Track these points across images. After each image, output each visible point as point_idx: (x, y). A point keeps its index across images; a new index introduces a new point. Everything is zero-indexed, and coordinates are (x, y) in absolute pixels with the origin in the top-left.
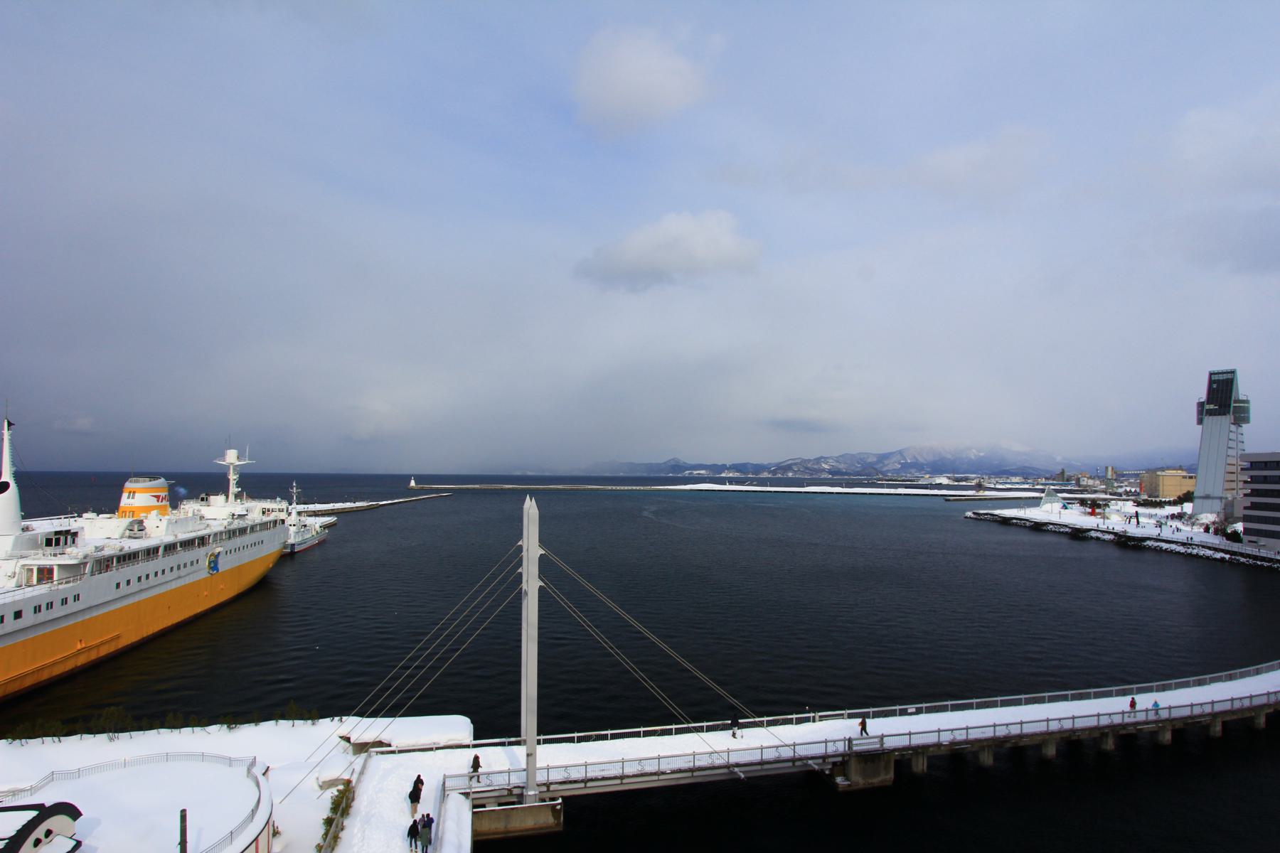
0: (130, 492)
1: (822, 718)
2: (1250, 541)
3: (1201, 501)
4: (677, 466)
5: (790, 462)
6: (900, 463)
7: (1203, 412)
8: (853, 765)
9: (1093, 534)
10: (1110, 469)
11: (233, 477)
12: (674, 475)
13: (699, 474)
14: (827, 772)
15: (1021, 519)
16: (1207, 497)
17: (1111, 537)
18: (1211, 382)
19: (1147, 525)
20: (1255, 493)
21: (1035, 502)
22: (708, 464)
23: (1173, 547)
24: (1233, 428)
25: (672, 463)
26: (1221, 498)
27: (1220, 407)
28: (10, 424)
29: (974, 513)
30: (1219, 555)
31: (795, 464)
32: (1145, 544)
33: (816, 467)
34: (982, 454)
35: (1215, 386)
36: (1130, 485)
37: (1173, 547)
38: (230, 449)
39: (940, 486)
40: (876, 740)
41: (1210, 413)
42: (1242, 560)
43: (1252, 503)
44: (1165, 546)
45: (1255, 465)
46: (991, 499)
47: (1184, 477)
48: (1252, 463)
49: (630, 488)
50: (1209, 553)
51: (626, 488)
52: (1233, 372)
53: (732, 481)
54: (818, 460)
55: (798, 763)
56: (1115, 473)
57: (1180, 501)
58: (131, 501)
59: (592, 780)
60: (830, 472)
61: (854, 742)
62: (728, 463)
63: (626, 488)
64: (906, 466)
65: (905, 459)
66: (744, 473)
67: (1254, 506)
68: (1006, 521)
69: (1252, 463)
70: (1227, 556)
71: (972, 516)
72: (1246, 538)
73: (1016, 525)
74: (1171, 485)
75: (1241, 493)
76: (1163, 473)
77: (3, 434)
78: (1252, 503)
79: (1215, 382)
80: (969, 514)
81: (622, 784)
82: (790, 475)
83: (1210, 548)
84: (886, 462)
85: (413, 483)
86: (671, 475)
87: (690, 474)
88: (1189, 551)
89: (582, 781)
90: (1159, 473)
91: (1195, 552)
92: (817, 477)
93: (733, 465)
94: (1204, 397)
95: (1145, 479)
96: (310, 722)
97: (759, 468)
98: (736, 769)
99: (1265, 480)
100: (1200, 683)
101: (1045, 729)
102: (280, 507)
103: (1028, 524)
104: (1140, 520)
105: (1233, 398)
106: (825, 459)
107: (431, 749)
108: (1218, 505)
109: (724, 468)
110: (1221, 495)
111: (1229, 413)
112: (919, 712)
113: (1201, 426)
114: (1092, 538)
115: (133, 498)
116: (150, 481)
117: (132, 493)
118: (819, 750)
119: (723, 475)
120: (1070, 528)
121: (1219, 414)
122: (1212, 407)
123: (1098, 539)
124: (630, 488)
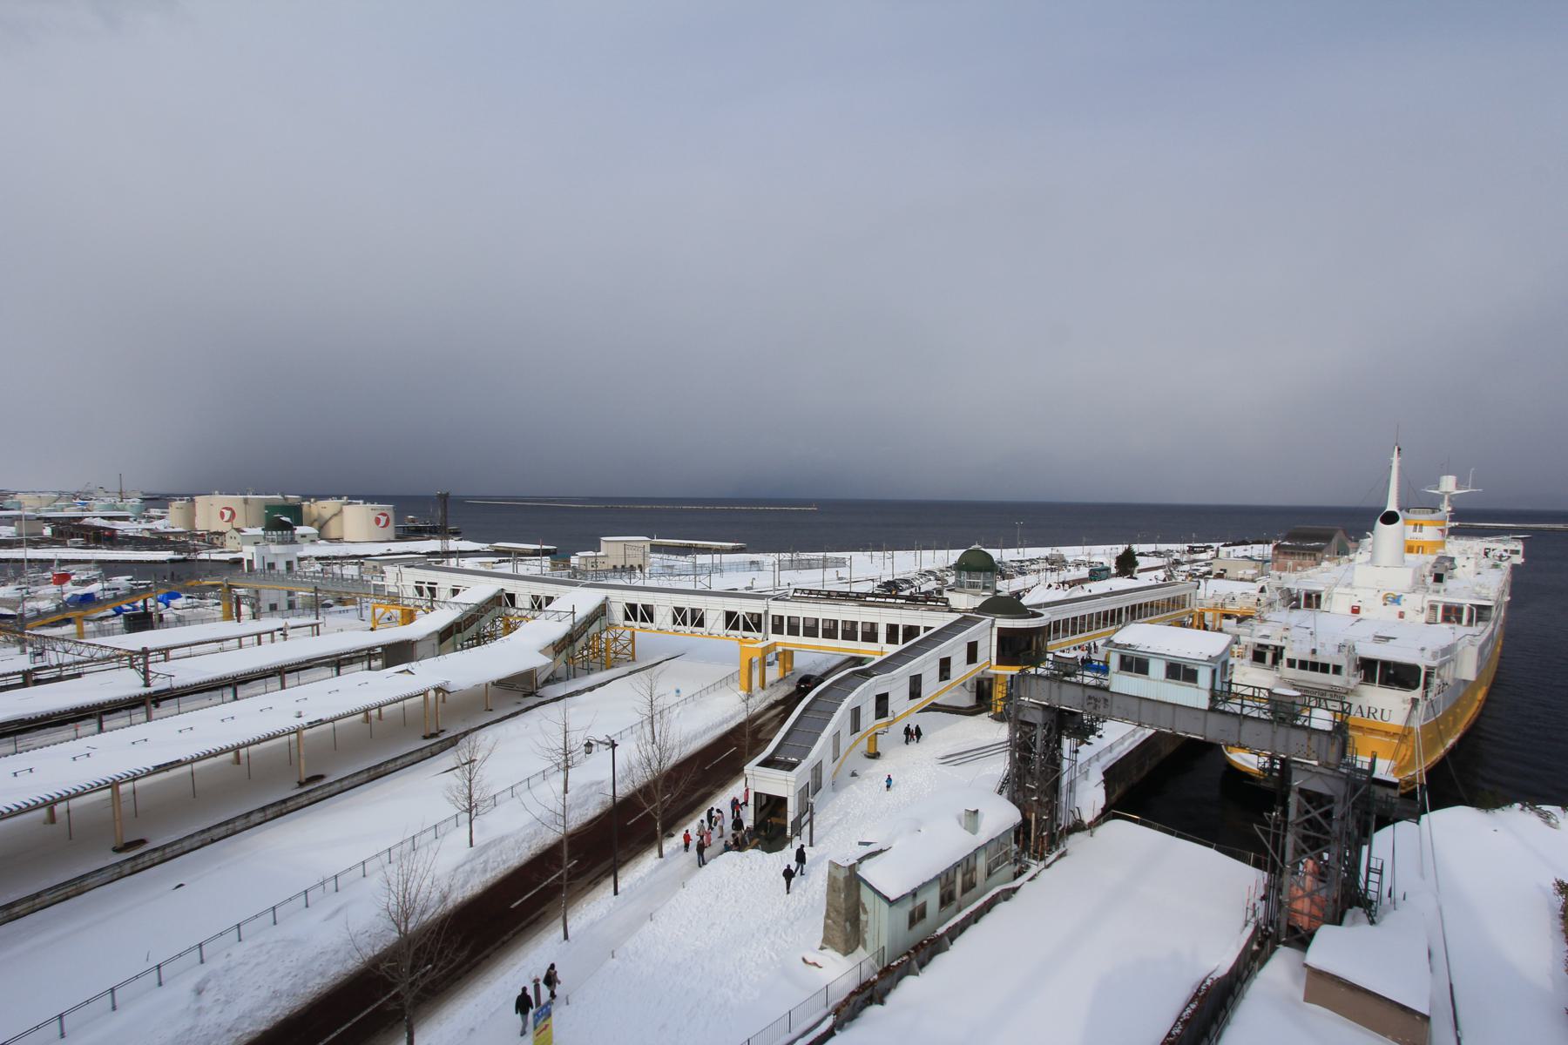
0: (1416, 525)
28: (1399, 449)
38: (1448, 474)
40: (21, 676)
58: (1417, 534)
107: (1456, 1027)
111: (1374, 682)
115: (1421, 531)
116: (1433, 512)
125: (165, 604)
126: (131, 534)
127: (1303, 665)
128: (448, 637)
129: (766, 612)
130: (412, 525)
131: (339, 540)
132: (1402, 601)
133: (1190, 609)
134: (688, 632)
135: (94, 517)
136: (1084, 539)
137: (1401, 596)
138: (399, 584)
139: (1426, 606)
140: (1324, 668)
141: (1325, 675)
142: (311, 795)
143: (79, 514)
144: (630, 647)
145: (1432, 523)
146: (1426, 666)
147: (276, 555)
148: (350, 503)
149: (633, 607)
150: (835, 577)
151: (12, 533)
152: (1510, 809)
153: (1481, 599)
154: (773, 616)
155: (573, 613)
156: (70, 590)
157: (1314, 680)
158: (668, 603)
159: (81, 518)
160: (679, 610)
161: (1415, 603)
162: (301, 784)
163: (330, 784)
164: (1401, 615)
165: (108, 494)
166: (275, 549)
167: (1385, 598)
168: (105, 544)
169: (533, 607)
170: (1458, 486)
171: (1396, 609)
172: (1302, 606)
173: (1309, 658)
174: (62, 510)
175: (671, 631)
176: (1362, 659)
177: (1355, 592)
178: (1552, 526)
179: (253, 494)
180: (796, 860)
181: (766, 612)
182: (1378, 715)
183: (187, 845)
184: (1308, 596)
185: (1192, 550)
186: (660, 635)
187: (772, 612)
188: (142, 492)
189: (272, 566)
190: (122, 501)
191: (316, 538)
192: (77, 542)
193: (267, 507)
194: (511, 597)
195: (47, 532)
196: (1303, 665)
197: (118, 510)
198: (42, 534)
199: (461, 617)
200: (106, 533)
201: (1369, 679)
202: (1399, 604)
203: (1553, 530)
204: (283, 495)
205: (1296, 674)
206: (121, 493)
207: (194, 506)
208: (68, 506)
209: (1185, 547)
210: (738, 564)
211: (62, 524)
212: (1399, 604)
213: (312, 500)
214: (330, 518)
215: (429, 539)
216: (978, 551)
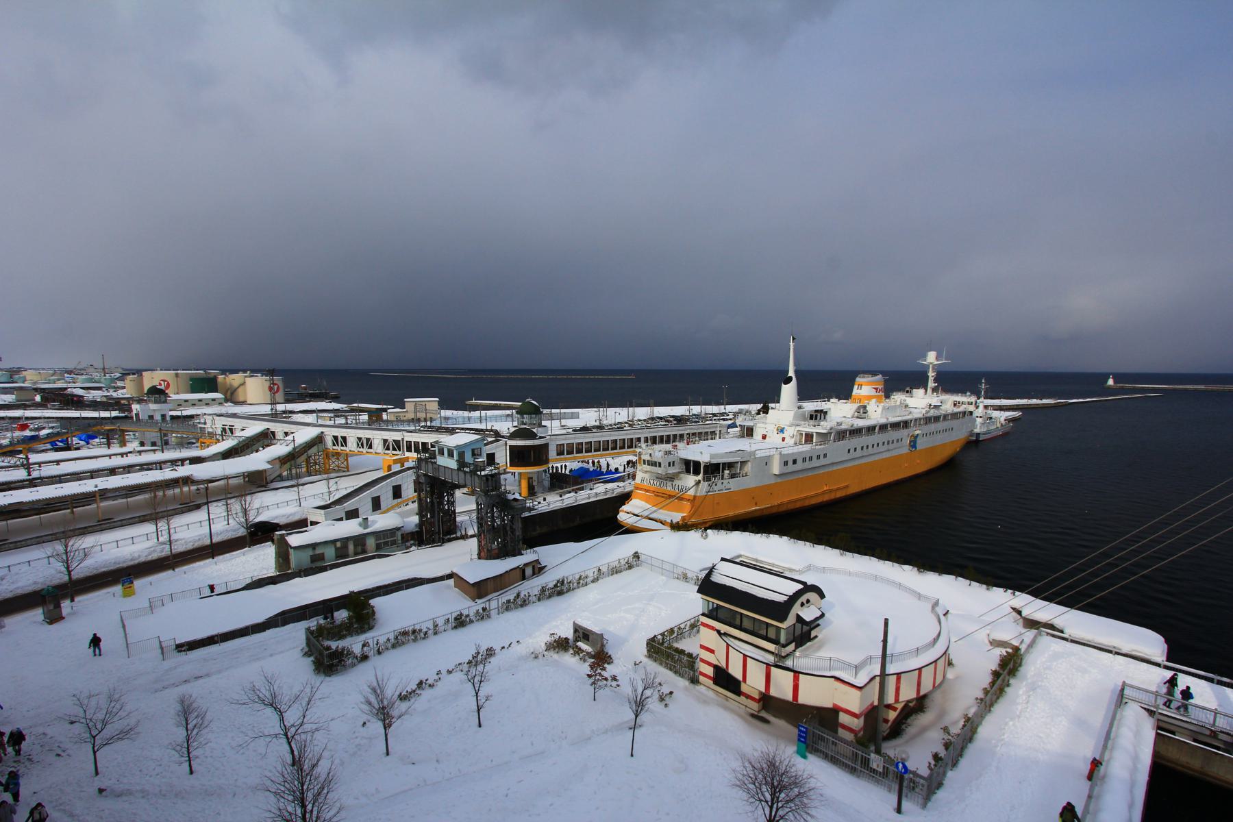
28: (794, 339)
77: (790, 345)
85: (1111, 382)
102: (969, 400)
111: (690, 473)
115: (861, 389)
117: (860, 386)
125: (86, 442)
126: (99, 400)
128: (227, 455)
129: (403, 439)
130: (303, 391)
131: (244, 403)
134: (365, 452)
135: (75, 388)
138: (213, 426)
142: (103, 526)
143: (65, 385)
144: (345, 463)
147: (154, 410)
148: (252, 376)
149: (336, 438)
150: (559, 425)
151: (13, 399)
154: (407, 442)
155: (294, 440)
156: (28, 433)
158: (353, 435)
159: (66, 389)
160: (360, 439)
161: (790, 431)
162: (99, 521)
163: (115, 522)
164: (784, 439)
165: (97, 370)
166: (153, 406)
167: (778, 429)
168: (73, 406)
169: (358, 445)
170: (937, 359)
171: (781, 435)
174: (54, 383)
175: (382, 453)
177: (766, 426)
178: (1195, 387)
179: (183, 370)
181: (403, 439)
183: (29, 542)
186: (377, 456)
187: (406, 439)
188: (123, 369)
189: (151, 417)
190: (105, 376)
191: (223, 401)
192: (55, 405)
193: (191, 379)
194: (344, 439)
195: (38, 398)
197: (96, 382)
198: (34, 400)
199: (238, 444)
200: (75, 399)
203: (1196, 390)
204: (205, 370)
206: (104, 369)
207: (142, 379)
208: (59, 380)
210: (496, 416)
211: (48, 393)
213: (227, 374)
214: (238, 387)
215: (310, 401)
216: (528, 402)
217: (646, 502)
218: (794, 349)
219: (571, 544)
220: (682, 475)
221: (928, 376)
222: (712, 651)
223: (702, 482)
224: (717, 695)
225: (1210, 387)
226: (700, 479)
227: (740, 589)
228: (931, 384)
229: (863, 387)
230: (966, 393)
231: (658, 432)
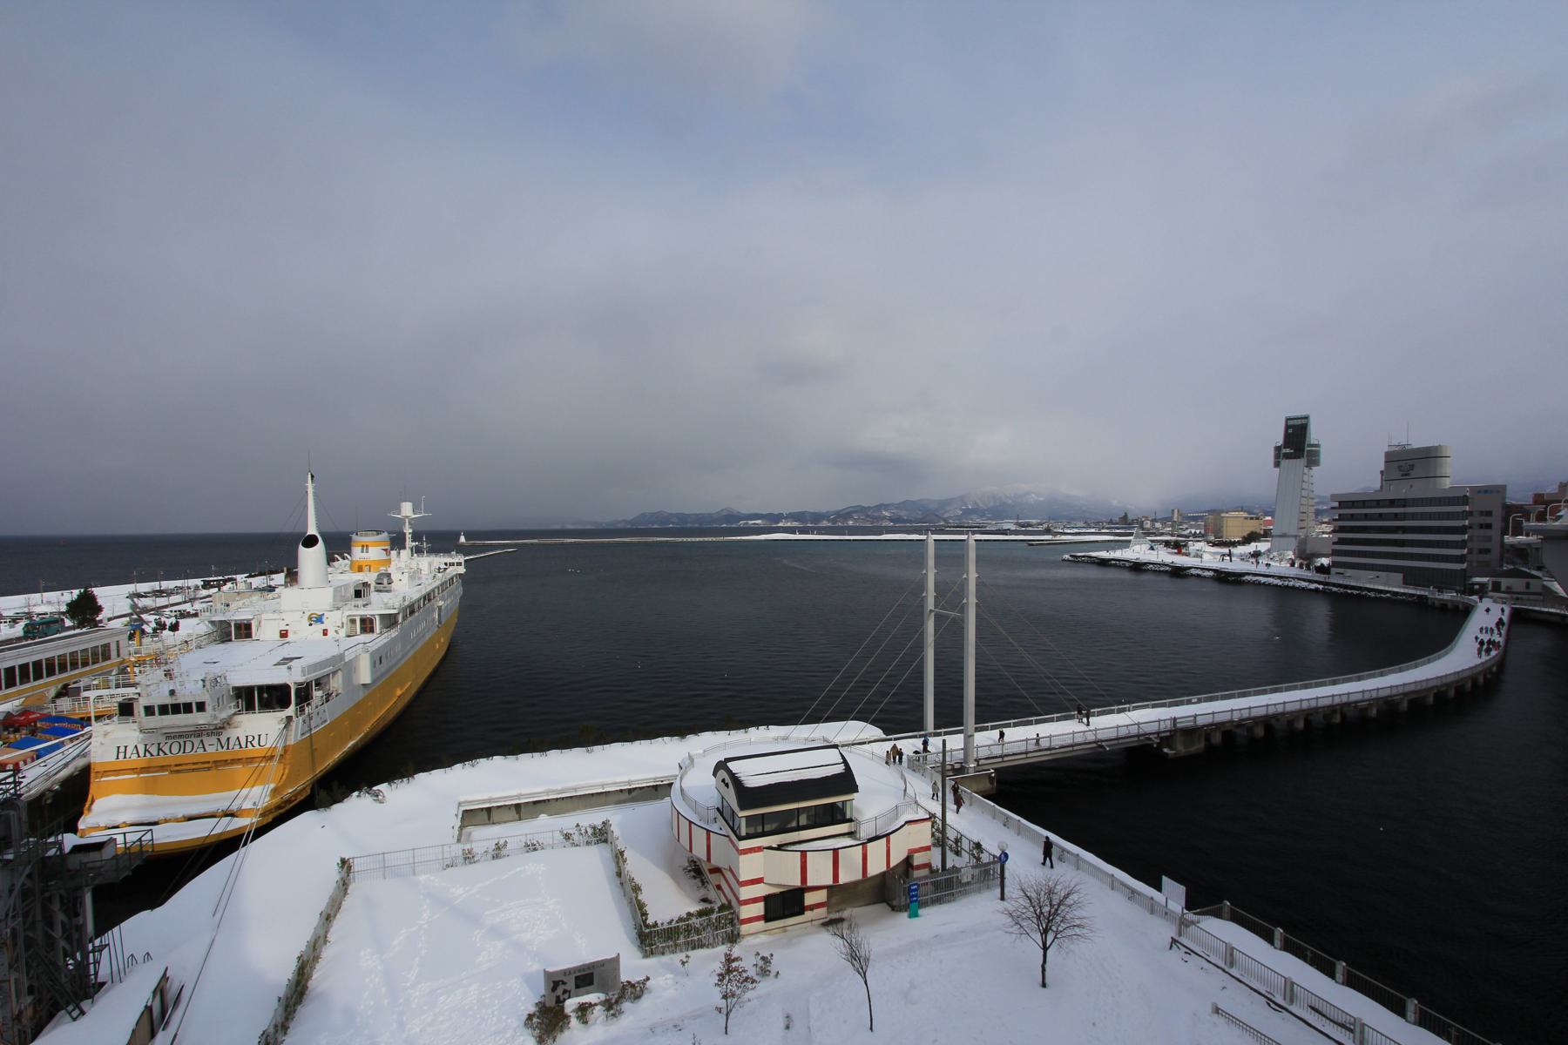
0: (363, 546)
1: (1135, 708)
2: (1337, 573)
3: (1278, 539)
4: (732, 517)
5: (849, 510)
6: (961, 510)
7: (1280, 455)
8: (1179, 740)
9: (1193, 571)
10: (1176, 511)
11: (408, 531)
12: (729, 526)
13: (755, 524)
14: (1155, 746)
15: (1119, 560)
16: (1283, 536)
17: (1211, 573)
18: (1287, 427)
19: (1237, 561)
20: (1342, 529)
21: (1126, 544)
22: (764, 513)
23: (1271, 580)
24: (1306, 470)
25: (725, 513)
26: (1295, 536)
27: (1295, 451)
28: (312, 476)
29: (1071, 556)
30: (1313, 586)
31: (855, 512)
32: (1244, 578)
33: (876, 514)
34: (1042, 499)
35: (1290, 431)
36: (1198, 527)
37: (1271, 580)
38: (406, 501)
39: (1005, 532)
41: (1287, 456)
42: (1335, 589)
43: (1339, 539)
44: (1263, 580)
45: (1342, 504)
46: (1071, 543)
47: (1246, 518)
48: (1340, 503)
49: (701, 539)
50: (1304, 584)
51: (698, 539)
52: (1307, 418)
53: (791, 530)
54: (879, 507)
55: (1141, 738)
56: (1181, 515)
57: (1248, 539)
58: (365, 555)
59: (1006, 756)
60: (891, 520)
61: (1178, 721)
62: (785, 512)
63: (698, 539)
64: (968, 512)
65: (966, 505)
66: (803, 523)
67: (1341, 541)
68: (1104, 563)
69: (1340, 503)
70: (1321, 587)
71: (1070, 558)
72: (1333, 570)
73: (1115, 566)
74: (1235, 526)
75: (1329, 528)
76: (1227, 515)
77: (307, 487)
78: (1339, 539)
79: (1291, 427)
80: (1067, 557)
81: (1027, 758)
82: (851, 523)
83: (1304, 580)
84: (947, 508)
85: (462, 539)
86: (724, 525)
87: (745, 524)
88: (1286, 583)
89: (1000, 757)
90: (1223, 515)
91: (1291, 584)
92: (879, 525)
93: (790, 513)
94: (1280, 441)
95: (1210, 521)
96: (743, 730)
97: (817, 517)
98: (1103, 744)
99: (1352, 517)
100: (1382, 675)
101: (1331, 703)
102: (457, 561)
103: (1127, 564)
104: (1233, 559)
105: (1307, 443)
106: (886, 507)
108: (1293, 543)
109: (779, 517)
110: (1295, 534)
112: (1199, 701)
113: (1278, 469)
114: (1192, 575)
115: (367, 552)
116: (378, 534)
117: (365, 547)
118: (1154, 728)
119: (780, 525)
120: (1170, 566)
121: (1295, 458)
122: (1288, 450)
123: (1198, 576)
124: (701, 539)
127: (164, 710)
132: (324, 619)
133: (119, 660)
136: (42, 584)
137: (323, 614)
139: (345, 621)
140: (187, 708)
141: (189, 715)
145: (377, 544)
146: (295, 683)
152: (679, 742)
153: (389, 609)
157: (178, 723)
161: (334, 619)
164: (325, 633)
167: (310, 618)
171: (319, 627)
172: (233, 638)
173: (169, 701)
176: (235, 689)
177: (283, 616)
180: (803, 914)
182: (255, 743)
184: (239, 626)
185: (207, 585)
196: (164, 710)
201: (250, 707)
202: (323, 623)
205: (158, 720)
209: (199, 582)
212: (323, 623)
217: (146, 793)
218: (315, 494)
219: (145, 915)
220: (239, 718)
221: (405, 533)
222: (760, 881)
223: (294, 719)
224: (770, 934)
225: (1117, 538)
226: (293, 714)
227: (790, 780)
228: (409, 543)
229: (370, 548)
230: (450, 553)
231: (32, 654)
